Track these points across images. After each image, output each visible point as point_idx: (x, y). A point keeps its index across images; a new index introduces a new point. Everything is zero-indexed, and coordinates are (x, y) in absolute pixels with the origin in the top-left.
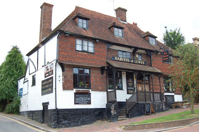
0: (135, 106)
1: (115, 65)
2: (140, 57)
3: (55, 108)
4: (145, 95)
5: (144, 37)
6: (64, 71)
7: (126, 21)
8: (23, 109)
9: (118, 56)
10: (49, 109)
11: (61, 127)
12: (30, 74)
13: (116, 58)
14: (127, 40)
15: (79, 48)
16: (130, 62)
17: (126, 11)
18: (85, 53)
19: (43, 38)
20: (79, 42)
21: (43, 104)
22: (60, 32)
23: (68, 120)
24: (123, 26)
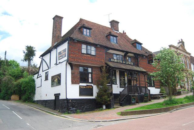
0: (126, 97)
1: (111, 64)
2: (130, 59)
3: (65, 98)
5: (132, 44)
7: (118, 31)
8: (37, 98)
9: (113, 58)
10: (60, 98)
12: (43, 71)
13: (112, 60)
14: (120, 46)
15: (84, 51)
16: (122, 63)
17: (118, 23)
18: (89, 56)
19: (55, 43)
20: (84, 46)
21: (55, 95)
22: (68, 38)
23: (75, 108)
24: (116, 35)
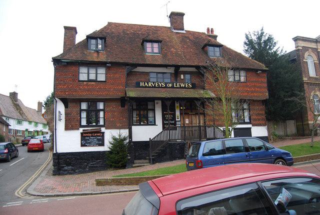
4: (200, 130)
6: (67, 108)
11: (63, 174)
15: (83, 77)
